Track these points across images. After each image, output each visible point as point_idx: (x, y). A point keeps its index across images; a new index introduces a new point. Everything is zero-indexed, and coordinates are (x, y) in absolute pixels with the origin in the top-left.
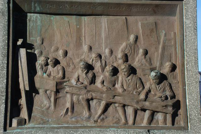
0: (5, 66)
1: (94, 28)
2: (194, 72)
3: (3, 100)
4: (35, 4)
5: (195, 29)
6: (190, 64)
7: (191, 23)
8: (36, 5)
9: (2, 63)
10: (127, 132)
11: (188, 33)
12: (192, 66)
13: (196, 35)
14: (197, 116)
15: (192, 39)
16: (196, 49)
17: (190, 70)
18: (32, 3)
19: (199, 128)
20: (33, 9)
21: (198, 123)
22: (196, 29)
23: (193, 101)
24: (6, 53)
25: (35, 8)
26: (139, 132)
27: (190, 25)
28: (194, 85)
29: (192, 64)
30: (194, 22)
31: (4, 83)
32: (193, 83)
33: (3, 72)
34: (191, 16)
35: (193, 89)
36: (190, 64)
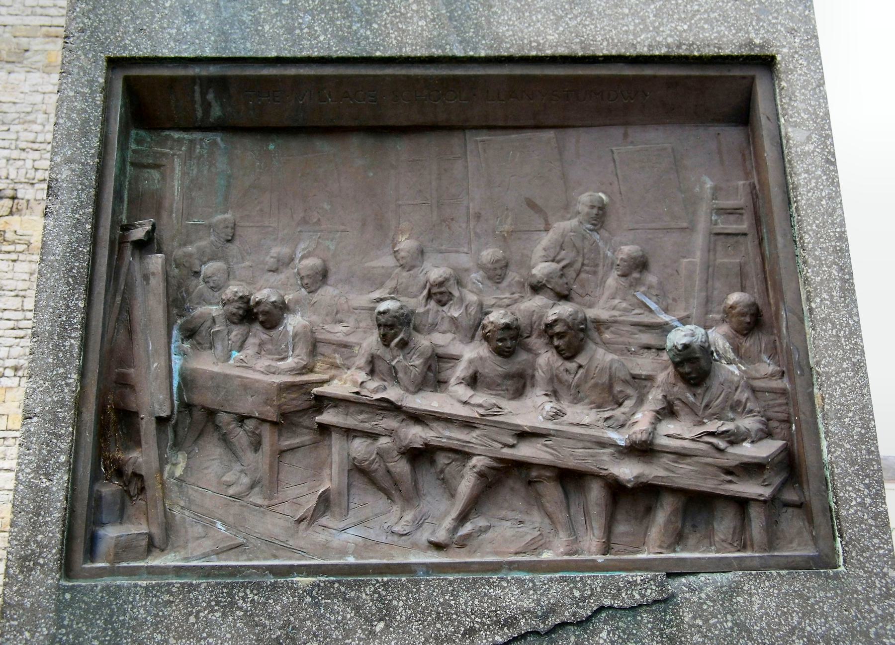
0: (78, 318)
1: (196, 488)
2: (841, 325)
3: (61, 452)
4: (203, 94)
5: (828, 161)
6: (825, 295)
7: (809, 138)
8: (210, 96)
9: (68, 307)
10: (579, 585)
11: (805, 178)
12: (832, 302)
13: (834, 182)
14: (870, 505)
15: (820, 199)
16: (842, 237)
17: (824, 320)
18: (194, 92)
19: (879, 556)
20: (199, 114)
21: (876, 535)
22: (830, 161)
23: (848, 446)
24: (84, 272)
25: (207, 106)
26: (629, 582)
27: (809, 147)
28: (849, 378)
29: (832, 297)
30: (821, 136)
31: (67, 385)
32: (844, 371)
33: (67, 344)
34: (809, 113)
35: (843, 395)
36: (825, 295)
